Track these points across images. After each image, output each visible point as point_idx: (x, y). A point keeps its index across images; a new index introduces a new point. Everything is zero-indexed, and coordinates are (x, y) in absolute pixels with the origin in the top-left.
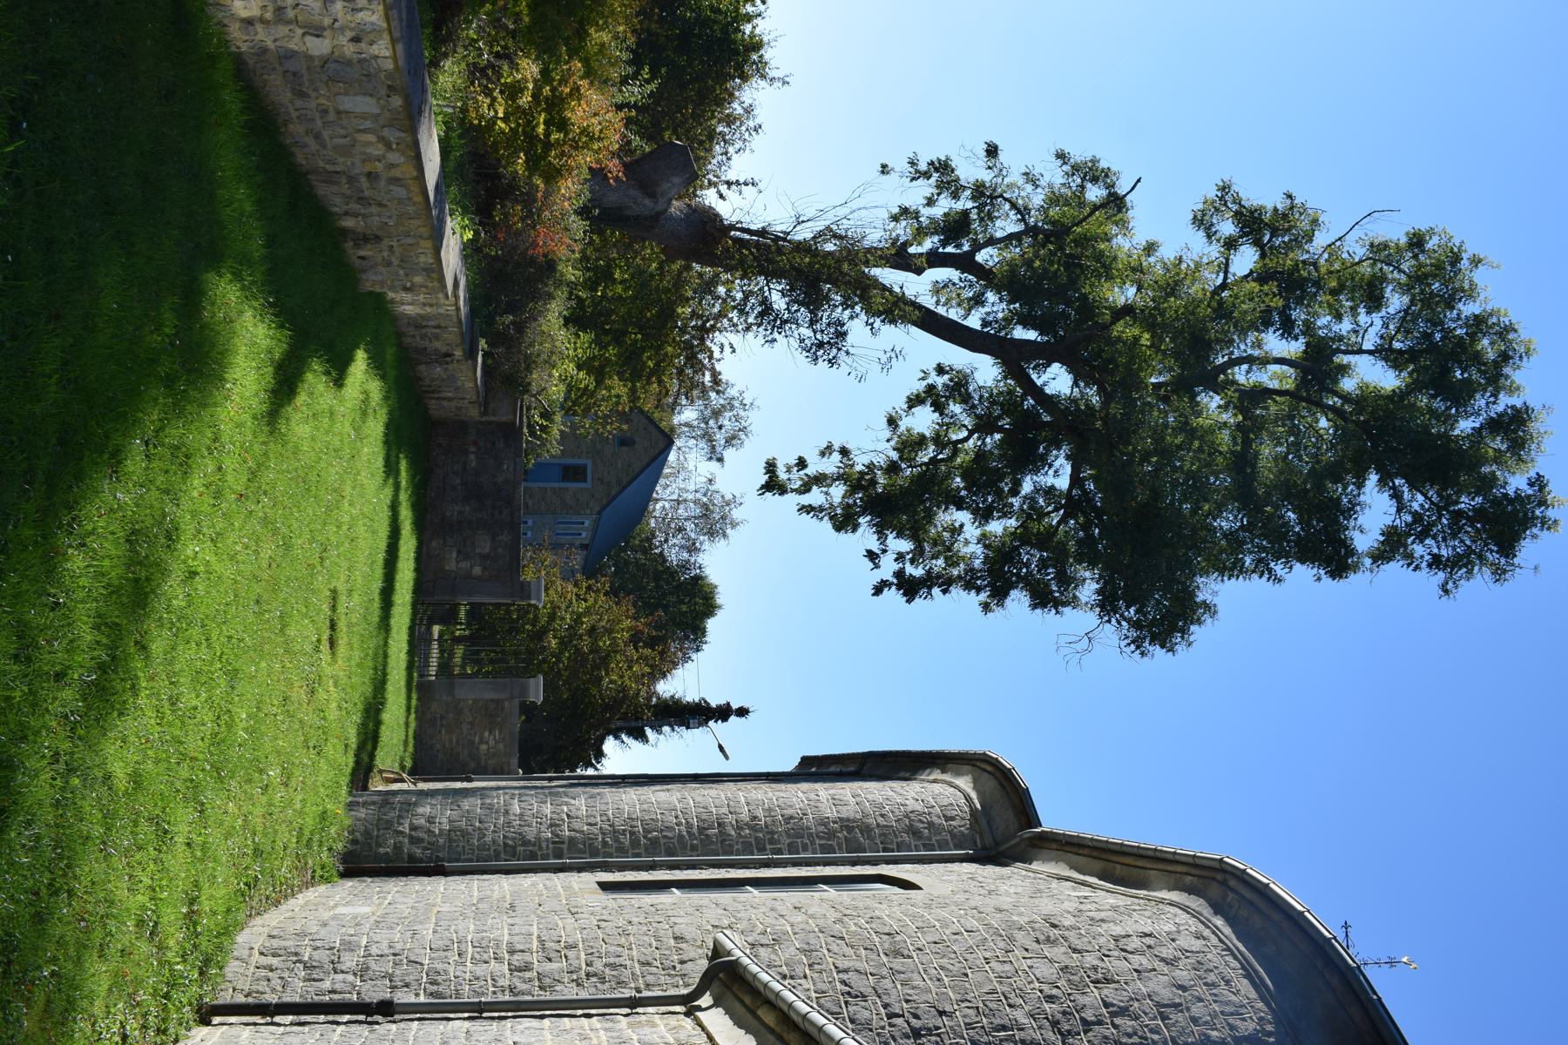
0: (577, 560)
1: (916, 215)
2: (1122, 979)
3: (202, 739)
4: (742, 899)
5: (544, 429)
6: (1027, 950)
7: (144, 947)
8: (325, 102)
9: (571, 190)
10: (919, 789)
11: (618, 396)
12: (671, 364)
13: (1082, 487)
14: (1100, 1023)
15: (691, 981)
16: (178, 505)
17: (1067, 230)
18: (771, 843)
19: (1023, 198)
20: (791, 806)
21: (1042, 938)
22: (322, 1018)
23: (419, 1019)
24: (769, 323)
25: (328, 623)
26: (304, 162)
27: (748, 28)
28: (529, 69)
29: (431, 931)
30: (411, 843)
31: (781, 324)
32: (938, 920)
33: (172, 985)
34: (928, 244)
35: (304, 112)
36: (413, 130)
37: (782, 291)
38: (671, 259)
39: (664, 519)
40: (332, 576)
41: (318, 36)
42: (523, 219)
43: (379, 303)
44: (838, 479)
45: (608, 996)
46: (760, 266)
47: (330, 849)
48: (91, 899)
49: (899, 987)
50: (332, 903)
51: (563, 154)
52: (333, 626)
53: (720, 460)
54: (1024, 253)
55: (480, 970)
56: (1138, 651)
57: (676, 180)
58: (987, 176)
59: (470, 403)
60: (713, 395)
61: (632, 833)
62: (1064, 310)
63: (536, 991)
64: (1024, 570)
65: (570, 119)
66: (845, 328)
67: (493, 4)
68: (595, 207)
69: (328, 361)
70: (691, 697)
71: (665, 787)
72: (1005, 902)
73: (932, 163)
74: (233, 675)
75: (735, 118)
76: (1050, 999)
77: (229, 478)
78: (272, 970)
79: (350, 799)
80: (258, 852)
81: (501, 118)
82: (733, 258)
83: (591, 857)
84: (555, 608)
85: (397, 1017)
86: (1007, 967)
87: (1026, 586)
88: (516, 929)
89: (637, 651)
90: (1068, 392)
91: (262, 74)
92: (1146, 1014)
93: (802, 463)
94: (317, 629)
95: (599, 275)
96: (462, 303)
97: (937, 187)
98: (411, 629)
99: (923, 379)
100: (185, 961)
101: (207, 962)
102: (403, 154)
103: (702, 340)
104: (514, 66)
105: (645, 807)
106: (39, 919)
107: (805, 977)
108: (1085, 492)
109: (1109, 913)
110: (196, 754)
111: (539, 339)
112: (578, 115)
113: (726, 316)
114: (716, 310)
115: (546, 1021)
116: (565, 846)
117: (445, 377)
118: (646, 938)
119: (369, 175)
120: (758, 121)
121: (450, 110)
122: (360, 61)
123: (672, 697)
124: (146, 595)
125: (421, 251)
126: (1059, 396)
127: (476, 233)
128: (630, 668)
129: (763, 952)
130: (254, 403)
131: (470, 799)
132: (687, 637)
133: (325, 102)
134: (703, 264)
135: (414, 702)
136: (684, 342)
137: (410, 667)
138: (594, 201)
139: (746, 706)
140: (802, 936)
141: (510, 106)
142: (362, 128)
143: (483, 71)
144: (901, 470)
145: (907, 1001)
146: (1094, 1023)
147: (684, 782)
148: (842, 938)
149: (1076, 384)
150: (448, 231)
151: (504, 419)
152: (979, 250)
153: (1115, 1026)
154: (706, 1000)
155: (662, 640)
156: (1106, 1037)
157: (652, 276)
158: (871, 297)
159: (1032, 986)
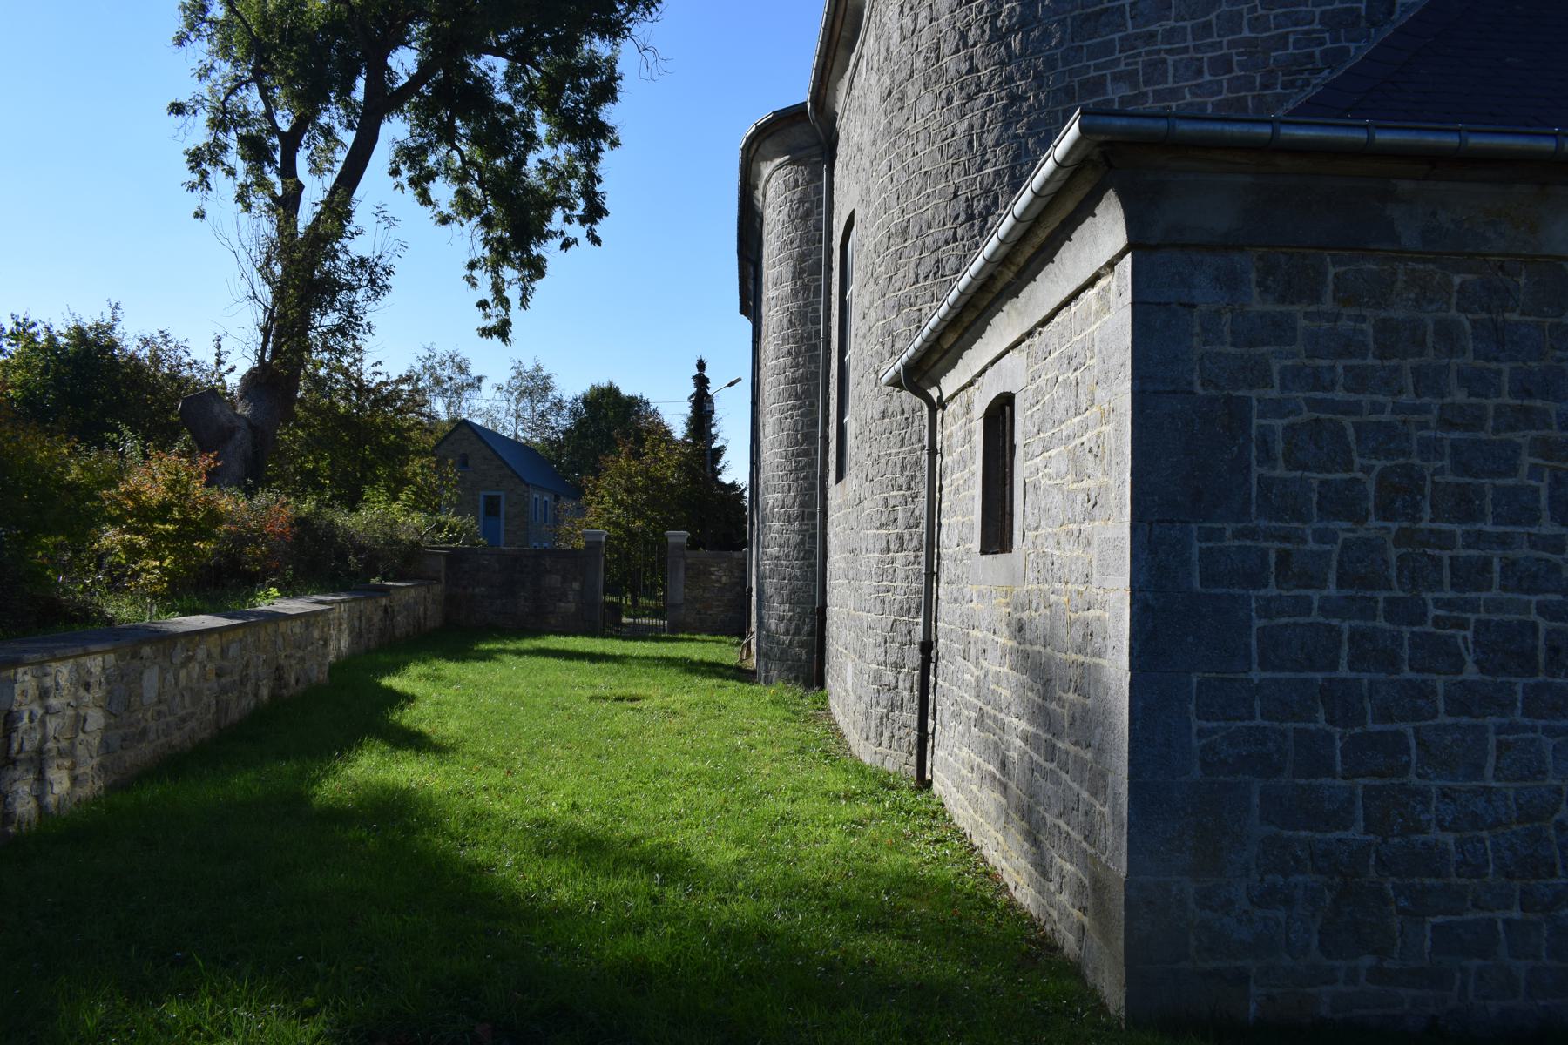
0: (570, 505)
1: (244, 187)
2: (937, 35)
3: (710, 794)
4: (855, 363)
5: (452, 530)
6: (908, 119)
7: (871, 830)
8: (149, 714)
9: (227, 502)
10: (770, 210)
11: (422, 467)
12: (392, 419)
13: (506, 46)
14: (971, 58)
15: (918, 405)
16: (516, 820)
17: (256, 40)
18: (811, 339)
19: (225, 82)
20: (781, 321)
21: (899, 105)
22: (931, 697)
23: (936, 622)
24: (352, 329)
25: (617, 703)
26: (209, 731)
27: (62, 341)
28: (111, 537)
29: (869, 615)
30: (799, 634)
31: (353, 317)
32: (880, 195)
33: (901, 809)
34: (273, 177)
35: (160, 732)
36: (174, 637)
37: (322, 316)
38: (294, 416)
39: (533, 430)
40: (579, 700)
41: (85, 720)
42: (258, 545)
43: (339, 668)
44: (497, 273)
45: (926, 473)
46: (298, 334)
47: (802, 697)
48: (832, 869)
49: (932, 231)
50: (844, 694)
51: (194, 507)
52: (621, 699)
53: (480, 379)
54: (280, 84)
55: (901, 575)
56: (657, 5)
57: (217, 409)
58: (204, 117)
59: (429, 592)
60: (421, 384)
61: (798, 456)
62: (336, 50)
63: (919, 530)
64: (582, 106)
65: (159, 501)
66: (356, 258)
67: (47, 569)
68: (245, 483)
69: (391, 707)
70: (687, 409)
71: (761, 428)
72: (868, 136)
73: (192, 169)
74: (659, 773)
75: (154, 355)
76: (949, 100)
77: (493, 782)
78: (893, 736)
79: (762, 683)
80: (802, 750)
81: (161, 563)
82: (290, 360)
83: (815, 489)
84: (609, 522)
85: (933, 639)
86: (921, 137)
87: (595, 105)
88: (871, 547)
89: (648, 453)
90: (415, 53)
91: (125, 768)
92: (966, 16)
93: (483, 304)
94: (623, 711)
95: (311, 481)
96: (338, 598)
97: (216, 165)
98: (625, 639)
99: (403, 188)
100: (883, 800)
101: (884, 785)
102: (197, 646)
103: (370, 391)
104: (110, 551)
105: (776, 444)
106: (845, 905)
107: (920, 310)
108: (510, 43)
109: (882, 43)
110: (722, 798)
111: (370, 533)
112: (154, 494)
113: (346, 368)
114: (341, 377)
115: (943, 521)
116: (806, 510)
117: (406, 613)
118: (882, 442)
119: (218, 675)
120: (156, 334)
121: (155, 609)
122: (108, 683)
123: (687, 425)
124: (591, 840)
125: (289, 632)
126: (420, 62)
127: (273, 585)
128: (661, 459)
129: (898, 345)
130: (428, 765)
131: (766, 587)
132: (637, 412)
133: (149, 714)
134: (297, 388)
135: (686, 636)
136: (372, 407)
137: (657, 639)
138: (239, 483)
139: (696, 362)
140: (887, 312)
141: (148, 554)
142: (173, 681)
143: (115, 580)
144: (489, 214)
145: (944, 224)
146: (971, 63)
147: (758, 412)
148: (891, 278)
149: (407, 44)
150: (271, 608)
151: (443, 563)
152: (278, 128)
153: (975, 44)
154: (934, 393)
155: (638, 432)
156: (983, 53)
157: (309, 435)
158: (326, 234)
159: (938, 116)
